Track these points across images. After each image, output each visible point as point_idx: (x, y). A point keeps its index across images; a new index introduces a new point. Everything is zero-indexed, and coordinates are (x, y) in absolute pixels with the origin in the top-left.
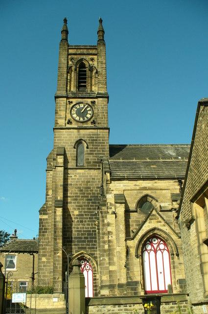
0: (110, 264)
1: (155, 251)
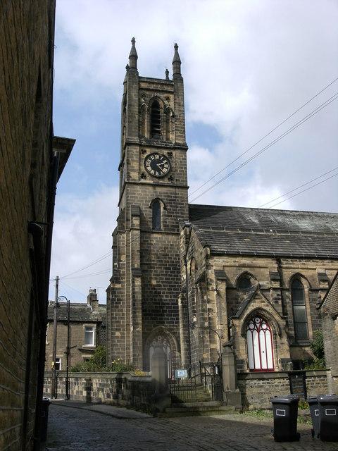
0: (211, 342)
1: (259, 332)
